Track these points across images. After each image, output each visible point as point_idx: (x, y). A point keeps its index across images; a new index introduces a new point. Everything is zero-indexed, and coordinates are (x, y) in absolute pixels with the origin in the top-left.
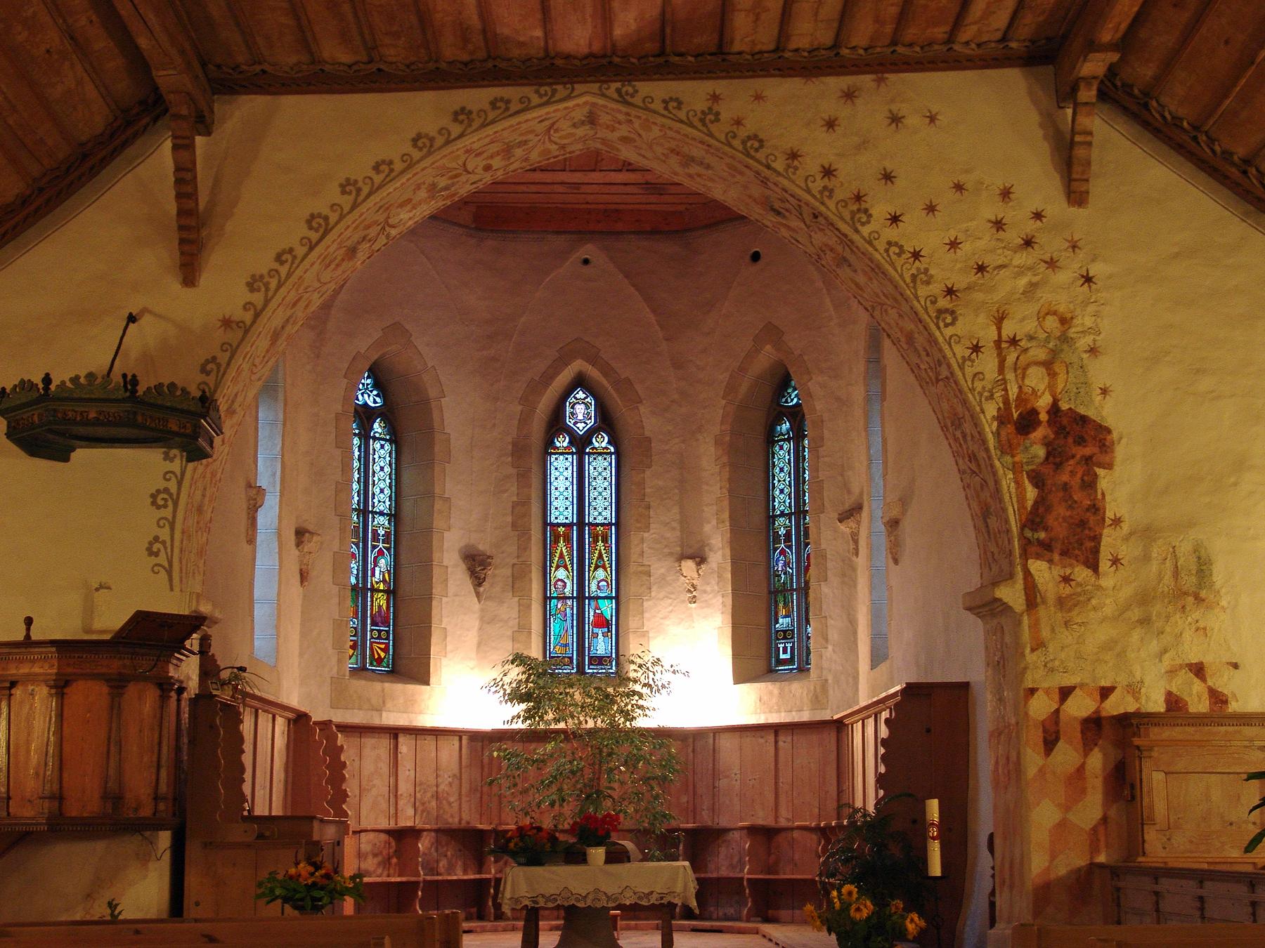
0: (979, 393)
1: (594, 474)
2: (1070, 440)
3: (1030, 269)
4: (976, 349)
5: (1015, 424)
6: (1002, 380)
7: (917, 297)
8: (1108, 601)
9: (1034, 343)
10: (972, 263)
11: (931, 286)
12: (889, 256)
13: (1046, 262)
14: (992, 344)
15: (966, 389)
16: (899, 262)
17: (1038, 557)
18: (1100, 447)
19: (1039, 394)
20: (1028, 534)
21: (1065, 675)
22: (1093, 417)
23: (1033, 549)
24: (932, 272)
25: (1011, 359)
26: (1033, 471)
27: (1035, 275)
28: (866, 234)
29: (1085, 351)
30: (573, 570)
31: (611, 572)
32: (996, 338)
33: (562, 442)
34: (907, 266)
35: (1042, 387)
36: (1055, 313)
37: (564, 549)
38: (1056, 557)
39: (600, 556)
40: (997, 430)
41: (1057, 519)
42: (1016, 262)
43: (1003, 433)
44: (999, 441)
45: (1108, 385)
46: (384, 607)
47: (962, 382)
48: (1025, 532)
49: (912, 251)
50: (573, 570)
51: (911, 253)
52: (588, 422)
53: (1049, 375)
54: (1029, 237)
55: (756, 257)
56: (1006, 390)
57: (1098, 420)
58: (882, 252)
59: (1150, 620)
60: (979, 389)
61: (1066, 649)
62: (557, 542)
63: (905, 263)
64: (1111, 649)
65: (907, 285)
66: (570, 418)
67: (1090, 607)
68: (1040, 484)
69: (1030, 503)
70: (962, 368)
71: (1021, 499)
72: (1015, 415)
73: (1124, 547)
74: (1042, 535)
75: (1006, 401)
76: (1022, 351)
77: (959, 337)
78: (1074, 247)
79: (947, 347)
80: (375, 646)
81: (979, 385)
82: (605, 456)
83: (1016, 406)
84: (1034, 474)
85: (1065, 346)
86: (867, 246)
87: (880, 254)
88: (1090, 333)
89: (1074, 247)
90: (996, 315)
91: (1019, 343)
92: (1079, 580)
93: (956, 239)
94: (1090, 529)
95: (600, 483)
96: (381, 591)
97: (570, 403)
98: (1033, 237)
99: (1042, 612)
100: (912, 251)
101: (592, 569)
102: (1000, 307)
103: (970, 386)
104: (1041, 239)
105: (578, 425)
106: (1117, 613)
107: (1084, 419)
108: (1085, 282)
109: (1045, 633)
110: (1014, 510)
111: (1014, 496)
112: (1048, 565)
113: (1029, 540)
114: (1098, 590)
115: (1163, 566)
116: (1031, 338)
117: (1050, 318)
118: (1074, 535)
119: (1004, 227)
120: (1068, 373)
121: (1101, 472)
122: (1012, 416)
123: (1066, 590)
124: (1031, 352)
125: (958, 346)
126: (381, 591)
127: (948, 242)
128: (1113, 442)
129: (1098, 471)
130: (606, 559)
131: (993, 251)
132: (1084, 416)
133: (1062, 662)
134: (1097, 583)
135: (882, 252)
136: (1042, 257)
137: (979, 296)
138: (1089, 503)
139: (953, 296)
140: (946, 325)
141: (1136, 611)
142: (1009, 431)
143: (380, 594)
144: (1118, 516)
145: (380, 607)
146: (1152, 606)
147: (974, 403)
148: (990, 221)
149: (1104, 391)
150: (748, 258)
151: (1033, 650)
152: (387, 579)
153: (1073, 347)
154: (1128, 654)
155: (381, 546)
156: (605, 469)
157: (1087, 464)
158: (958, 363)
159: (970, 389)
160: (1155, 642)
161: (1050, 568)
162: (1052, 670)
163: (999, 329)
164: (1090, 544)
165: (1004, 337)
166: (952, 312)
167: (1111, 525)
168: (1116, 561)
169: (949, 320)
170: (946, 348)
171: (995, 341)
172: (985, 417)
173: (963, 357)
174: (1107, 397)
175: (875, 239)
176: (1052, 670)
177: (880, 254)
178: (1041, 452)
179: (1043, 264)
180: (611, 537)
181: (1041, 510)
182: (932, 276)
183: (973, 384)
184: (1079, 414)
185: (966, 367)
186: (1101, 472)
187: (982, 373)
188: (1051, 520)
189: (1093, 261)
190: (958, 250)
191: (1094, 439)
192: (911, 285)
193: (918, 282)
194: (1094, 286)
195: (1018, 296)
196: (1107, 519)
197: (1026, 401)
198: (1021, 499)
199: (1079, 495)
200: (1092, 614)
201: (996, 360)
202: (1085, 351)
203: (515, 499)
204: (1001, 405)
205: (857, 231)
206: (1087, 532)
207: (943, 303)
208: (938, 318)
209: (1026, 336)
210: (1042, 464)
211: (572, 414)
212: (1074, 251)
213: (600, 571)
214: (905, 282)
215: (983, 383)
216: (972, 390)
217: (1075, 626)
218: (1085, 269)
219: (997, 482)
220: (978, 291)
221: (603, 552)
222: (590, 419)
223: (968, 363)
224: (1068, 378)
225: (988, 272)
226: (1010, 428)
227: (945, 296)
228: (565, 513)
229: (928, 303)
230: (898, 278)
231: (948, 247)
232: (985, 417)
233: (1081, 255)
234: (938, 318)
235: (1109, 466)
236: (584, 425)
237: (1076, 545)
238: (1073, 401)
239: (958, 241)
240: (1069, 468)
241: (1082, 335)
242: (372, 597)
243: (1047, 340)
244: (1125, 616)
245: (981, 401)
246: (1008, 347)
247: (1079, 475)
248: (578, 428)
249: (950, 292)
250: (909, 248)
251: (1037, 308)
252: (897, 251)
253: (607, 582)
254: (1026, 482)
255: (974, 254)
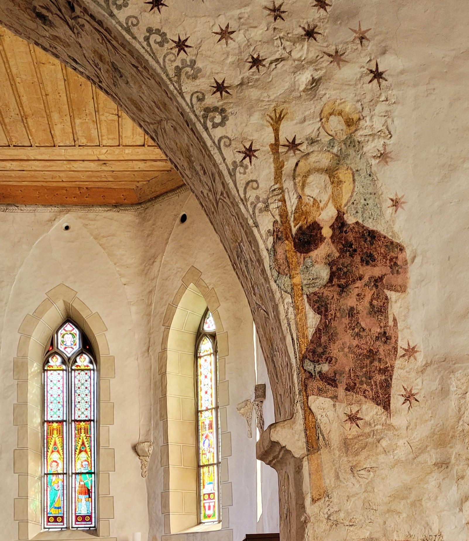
0: (252, 203)
1: (78, 384)
2: (357, 259)
3: (311, 63)
4: (249, 153)
5: (294, 241)
6: (279, 189)
7: (181, 94)
8: (401, 443)
9: (315, 147)
10: (245, 56)
11: (197, 82)
12: (149, 45)
13: (330, 55)
14: (268, 148)
15: (238, 199)
16: (161, 52)
17: (320, 392)
18: (391, 268)
19: (321, 205)
20: (309, 366)
21: (351, 528)
22: (384, 233)
23: (314, 384)
24: (199, 64)
25: (289, 165)
26: (315, 294)
27: (316, 70)
28: (123, 20)
29: (374, 157)
30: (63, 454)
31: (91, 455)
32: (273, 141)
33: (55, 362)
34: (171, 57)
35: (325, 197)
36: (340, 114)
37: (57, 439)
38: (341, 391)
39: (83, 444)
40: (274, 247)
41: (343, 349)
42: (296, 55)
43: (280, 251)
44: (276, 260)
45: (399, 197)
47: (234, 192)
48: (305, 365)
49: (177, 40)
50: (63, 454)
51: (175, 42)
52: (74, 347)
53: (332, 183)
54: (312, 27)
55: (184, 219)
56: (283, 201)
57: (389, 236)
58: (141, 39)
59: (449, 463)
60: (252, 199)
61: (353, 499)
62: (52, 433)
63: (167, 54)
64: (404, 498)
65: (170, 79)
66: (61, 345)
67: (380, 449)
68: (323, 309)
69: (310, 332)
70: (232, 175)
71: (301, 327)
72: (294, 230)
73: (419, 381)
74: (325, 368)
75: (284, 215)
76: (302, 157)
77: (230, 140)
78: (362, 38)
79: (216, 151)
81: (252, 195)
82: (86, 372)
83: (295, 219)
84: (316, 298)
85: (351, 151)
86: (124, 33)
87: (139, 43)
88: (379, 136)
89: (362, 38)
90: (273, 115)
91: (299, 147)
92: (367, 418)
93: (227, 27)
94: (380, 360)
95: (83, 391)
97: (61, 334)
98: (316, 26)
99: (324, 455)
100: (177, 40)
101: (77, 453)
102: (277, 106)
103: (242, 196)
104: (325, 29)
105: (67, 350)
106: (411, 456)
107: (373, 235)
108: (375, 77)
109: (329, 481)
110: (293, 339)
111: (292, 323)
112: (332, 403)
113: (309, 373)
114: (389, 430)
115: (462, 401)
116: (312, 142)
117: (332, 118)
118: (362, 368)
119: (283, 15)
120: (354, 181)
121: (392, 295)
122: (291, 230)
123: (352, 431)
124: (312, 159)
125: (229, 149)
127: (219, 31)
128: (406, 261)
129: (388, 293)
130: (87, 446)
131: (270, 41)
132: (373, 231)
133: (348, 513)
134: (388, 422)
135: (141, 39)
136: (325, 50)
137: (253, 93)
138: (379, 330)
139: (224, 93)
140: (215, 126)
141: (433, 452)
142: (287, 248)
144: (412, 345)
146: (451, 447)
147: (246, 215)
148: (266, 8)
149: (396, 203)
150: (178, 220)
151: (314, 501)
153: (361, 152)
154: (423, 503)
156: (86, 381)
157: (377, 287)
158: (229, 170)
159: (242, 200)
160: (455, 488)
161: (334, 405)
162: (336, 523)
163: (276, 131)
164: (379, 378)
165: (282, 140)
166: (222, 111)
167: (404, 356)
168: (409, 397)
169: (218, 119)
170: (214, 152)
171: (271, 145)
172: (259, 231)
173: (235, 162)
174: (400, 209)
175: (134, 25)
176: (336, 523)
177: (139, 43)
178: (324, 273)
179: (326, 57)
180: (91, 429)
181: (324, 339)
182: (199, 70)
183: (245, 193)
184: (367, 229)
185: (238, 174)
186: (392, 295)
187: (256, 181)
188: (334, 350)
189: (384, 53)
190: (230, 41)
191: (385, 257)
192: (175, 79)
193: (183, 76)
194: (383, 83)
195: (297, 94)
196: (399, 349)
197: (306, 214)
198: (301, 327)
199: (368, 321)
200: (382, 458)
201: (272, 166)
202: (374, 157)
203: (16, 402)
204: (278, 218)
205: (112, 15)
206: (376, 363)
207: (212, 100)
208: (205, 117)
209: (307, 139)
210: (325, 286)
211: (63, 342)
212: (361, 42)
213: (83, 454)
214: (167, 75)
215: (257, 192)
216: (244, 201)
217: (362, 472)
218: (373, 63)
219: (276, 308)
220: (252, 86)
221: (85, 440)
222: (75, 345)
223: (240, 169)
224: (354, 187)
225: (264, 66)
226: (288, 245)
227: (214, 93)
228: (52, 413)
229: (194, 100)
230: (159, 70)
231: (219, 37)
232: (259, 231)
233: (371, 46)
234: (205, 117)
235: (402, 289)
236: (71, 349)
237: (364, 379)
238: (360, 214)
239: (229, 30)
240: (356, 291)
241: (371, 138)
243: (331, 143)
244: (419, 459)
245: (254, 213)
246: (287, 152)
247: (368, 299)
248: (67, 352)
249: (220, 88)
250: (173, 36)
251: (319, 108)
252: (159, 39)
253: (88, 462)
254: (307, 306)
255: (249, 46)
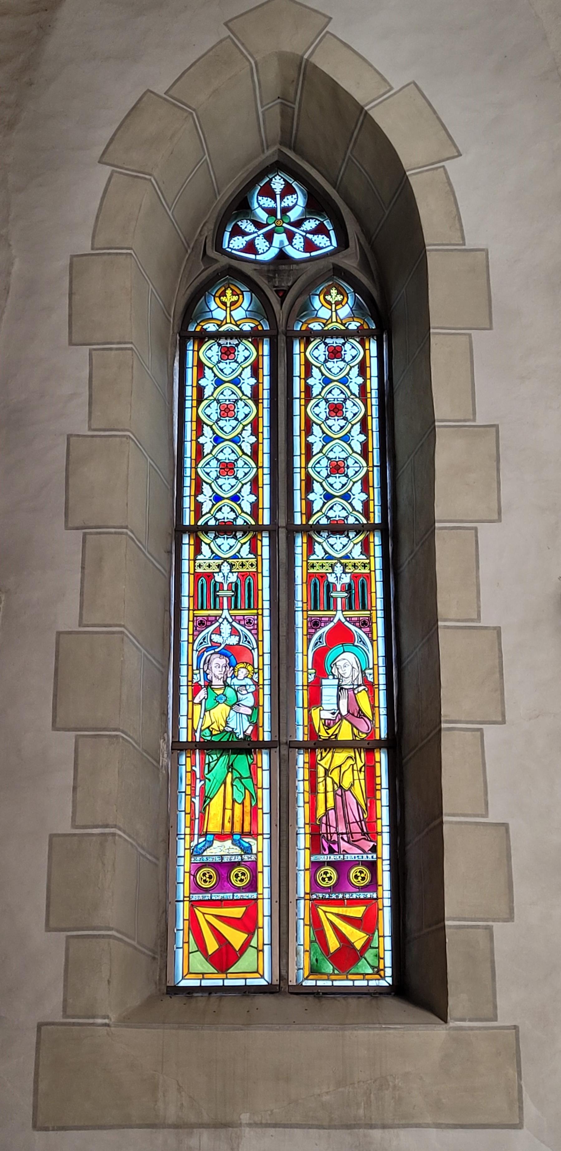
46: (359, 791)
80: (201, 913)
96: (344, 745)
126: (344, 745)
143: (340, 757)
145: (341, 792)
152: (366, 709)
155: (339, 616)
242: (313, 766)
